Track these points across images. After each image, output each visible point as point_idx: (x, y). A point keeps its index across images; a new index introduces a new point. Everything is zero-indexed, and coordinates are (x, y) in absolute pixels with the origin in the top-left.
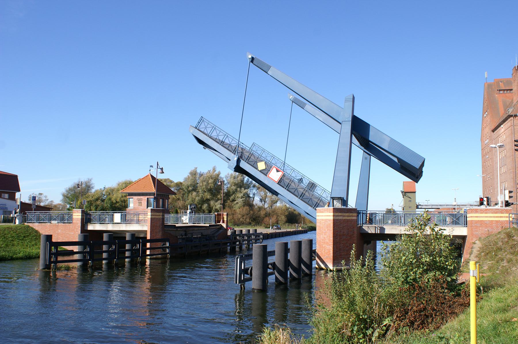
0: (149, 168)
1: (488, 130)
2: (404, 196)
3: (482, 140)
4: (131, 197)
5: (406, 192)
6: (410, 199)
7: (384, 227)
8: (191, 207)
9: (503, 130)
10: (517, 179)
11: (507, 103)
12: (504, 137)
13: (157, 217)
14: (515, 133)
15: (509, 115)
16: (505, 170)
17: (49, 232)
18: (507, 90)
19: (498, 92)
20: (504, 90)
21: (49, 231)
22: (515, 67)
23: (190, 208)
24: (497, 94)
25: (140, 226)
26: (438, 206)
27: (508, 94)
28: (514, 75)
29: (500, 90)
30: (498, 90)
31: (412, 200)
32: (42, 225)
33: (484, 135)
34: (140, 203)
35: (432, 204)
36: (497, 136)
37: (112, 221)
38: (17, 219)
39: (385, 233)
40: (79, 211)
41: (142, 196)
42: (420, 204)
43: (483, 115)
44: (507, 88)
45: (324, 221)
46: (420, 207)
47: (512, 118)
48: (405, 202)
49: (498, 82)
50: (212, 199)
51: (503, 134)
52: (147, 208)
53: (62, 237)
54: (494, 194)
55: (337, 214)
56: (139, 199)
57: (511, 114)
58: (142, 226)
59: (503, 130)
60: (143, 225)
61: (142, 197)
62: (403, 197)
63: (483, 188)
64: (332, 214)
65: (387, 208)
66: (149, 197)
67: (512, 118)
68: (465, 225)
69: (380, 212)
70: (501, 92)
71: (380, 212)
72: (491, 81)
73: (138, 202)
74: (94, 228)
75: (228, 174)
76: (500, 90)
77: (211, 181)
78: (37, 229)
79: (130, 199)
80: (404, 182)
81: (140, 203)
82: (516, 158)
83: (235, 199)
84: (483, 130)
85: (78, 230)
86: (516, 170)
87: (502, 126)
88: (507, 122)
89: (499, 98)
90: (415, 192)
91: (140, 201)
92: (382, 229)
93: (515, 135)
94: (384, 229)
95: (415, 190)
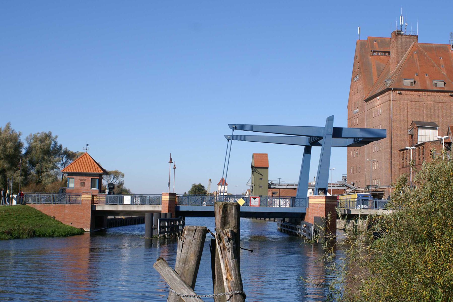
0: (86, 147)
1: (359, 97)
2: (254, 172)
3: (349, 107)
4: (72, 177)
5: (256, 168)
6: (261, 177)
7: (350, 209)
8: (110, 187)
9: (378, 102)
10: (392, 160)
11: (381, 68)
12: (379, 111)
13: (87, 199)
14: (393, 108)
15: (388, 88)
16: (379, 149)
17: (54, 212)
18: (382, 52)
19: (372, 53)
20: (378, 52)
21: (54, 211)
22: (395, 32)
23: (108, 189)
24: (370, 55)
25: (152, 207)
26: (294, 186)
27: (383, 57)
28: (393, 40)
29: (374, 51)
30: (372, 51)
31: (264, 178)
32: (45, 205)
33: (353, 103)
34: (83, 184)
35: (287, 183)
36: (371, 107)
37: (122, 203)
38: (13, 200)
39: (351, 213)
40: (88, 193)
41: (85, 176)
42: (272, 182)
43: (353, 79)
44: (382, 50)
45: (316, 205)
46: (272, 186)
47: (391, 91)
48: (255, 181)
49: (372, 40)
50: (9, 169)
51: (379, 107)
52: (91, 189)
53: (69, 216)
54: (364, 174)
55: (328, 200)
56: (82, 179)
57: (390, 87)
58: (153, 207)
59: (378, 102)
60: (154, 207)
61: (85, 178)
62: (253, 173)
63: (348, 166)
64: (325, 200)
65: (194, 183)
66: (93, 177)
67: (391, 91)
68: (375, 208)
69: (347, 199)
70: (375, 54)
71: (347, 199)
72: (364, 38)
73: (80, 182)
74: (102, 209)
75: (31, 136)
76: (374, 51)
77: (9, 145)
78: (39, 209)
79: (70, 179)
80: (254, 154)
81: (83, 184)
82: (392, 137)
83: (41, 169)
84: (351, 95)
85: (88, 210)
86: (392, 150)
87: (378, 98)
88: (384, 94)
89: (373, 60)
90: (267, 168)
91: (83, 182)
92: (349, 211)
93: (393, 111)
94: (350, 211)
95: (268, 165)
